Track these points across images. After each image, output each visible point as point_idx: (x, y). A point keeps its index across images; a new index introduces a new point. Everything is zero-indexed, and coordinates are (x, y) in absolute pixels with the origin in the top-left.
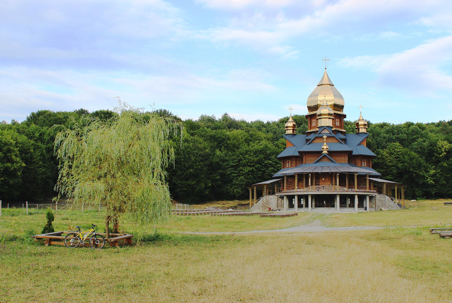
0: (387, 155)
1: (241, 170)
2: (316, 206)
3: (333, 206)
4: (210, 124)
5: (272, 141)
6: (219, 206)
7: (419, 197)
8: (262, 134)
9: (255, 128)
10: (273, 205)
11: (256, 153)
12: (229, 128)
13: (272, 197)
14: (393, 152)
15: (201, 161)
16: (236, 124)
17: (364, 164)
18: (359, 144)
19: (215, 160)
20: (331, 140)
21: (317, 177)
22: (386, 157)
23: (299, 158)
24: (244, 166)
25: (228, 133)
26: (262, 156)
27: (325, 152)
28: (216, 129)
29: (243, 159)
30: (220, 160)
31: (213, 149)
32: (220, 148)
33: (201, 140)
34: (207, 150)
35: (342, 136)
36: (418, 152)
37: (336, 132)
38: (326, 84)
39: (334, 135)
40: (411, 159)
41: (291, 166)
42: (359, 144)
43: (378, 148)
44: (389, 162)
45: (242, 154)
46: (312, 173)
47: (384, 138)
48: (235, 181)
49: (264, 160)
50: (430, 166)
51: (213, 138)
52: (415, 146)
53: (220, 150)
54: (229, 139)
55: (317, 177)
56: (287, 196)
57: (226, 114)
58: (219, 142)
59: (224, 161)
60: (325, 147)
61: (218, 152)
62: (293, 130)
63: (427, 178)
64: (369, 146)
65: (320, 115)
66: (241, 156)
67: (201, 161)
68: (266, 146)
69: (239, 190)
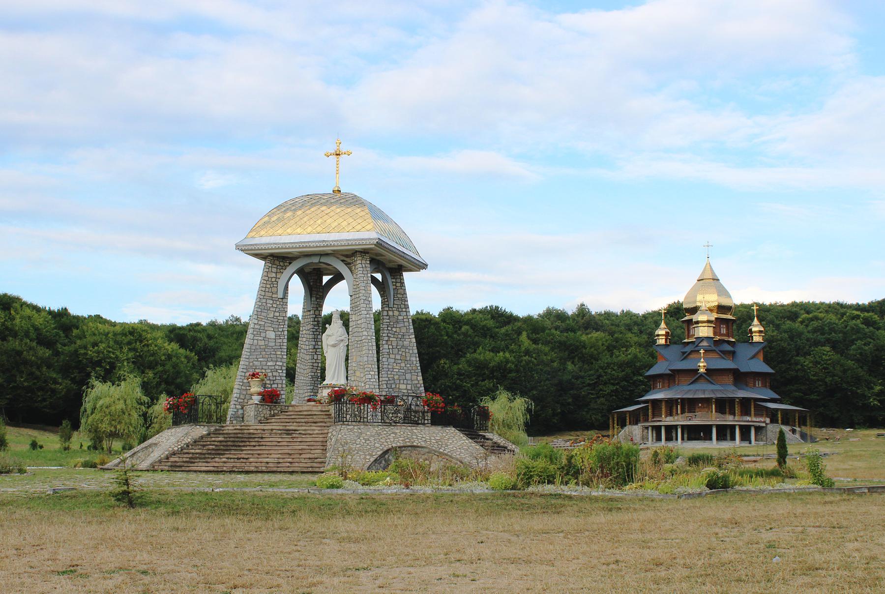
0: (811, 365)
1: (601, 390)
2: (689, 439)
3: (711, 439)
4: (558, 323)
5: (645, 347)
6: (572, 438)
7: (858, 424)
8: (631, 337)
9: (623, 328)
10: (637, 438)
11: (622, 365)
12: (586, 328)
13: (635, 427)
14: (818, 359)
15: (547, 379)
16: (596, 323)
17: (759, 384)
18: (752, 358)
19: (566, 377)
20: (711, 355)
21: (690, 405)
22: (809, 368)
23: (671, 378)
24: (605, 384)
25: (584, 338)
26: (628, 370)
27: (702, 370)
28: (567, 330)
29: (603, 374)
30: (573, 377)
31: (563, 361)
32: (571, 358)
33: (547, 349)
34: (555, 364)
35: (728, 348)
36: (858, 361)
37: (717, 343)
38: (709, 280)
39: (714, 348)
40: (845, 371)
41: (663, 387)
42: (752, 358)
43: (797, 356)
44: (814, 375)
45: (601, 368)
46: (682, 399)
47: (808, 340)
48: (592, 405)
49: (632, 375)
50: (875, 380)
51: (562, 346)
52: (851, 352)
53: (573, 363)
54: (584, 347)
55: (690, 405)
56: (653, 427)
57: (583, 305)
58: (572, 351)
59: (577, 378)
60: (701, 364)
61: (570, 366)
62: (666, 340)
63: (869, 398)
64: (767, 361)
65: (697, 322)
66: (600, 370)
67: (547, 379)
68: (636, 357)
69: (599, 417)
